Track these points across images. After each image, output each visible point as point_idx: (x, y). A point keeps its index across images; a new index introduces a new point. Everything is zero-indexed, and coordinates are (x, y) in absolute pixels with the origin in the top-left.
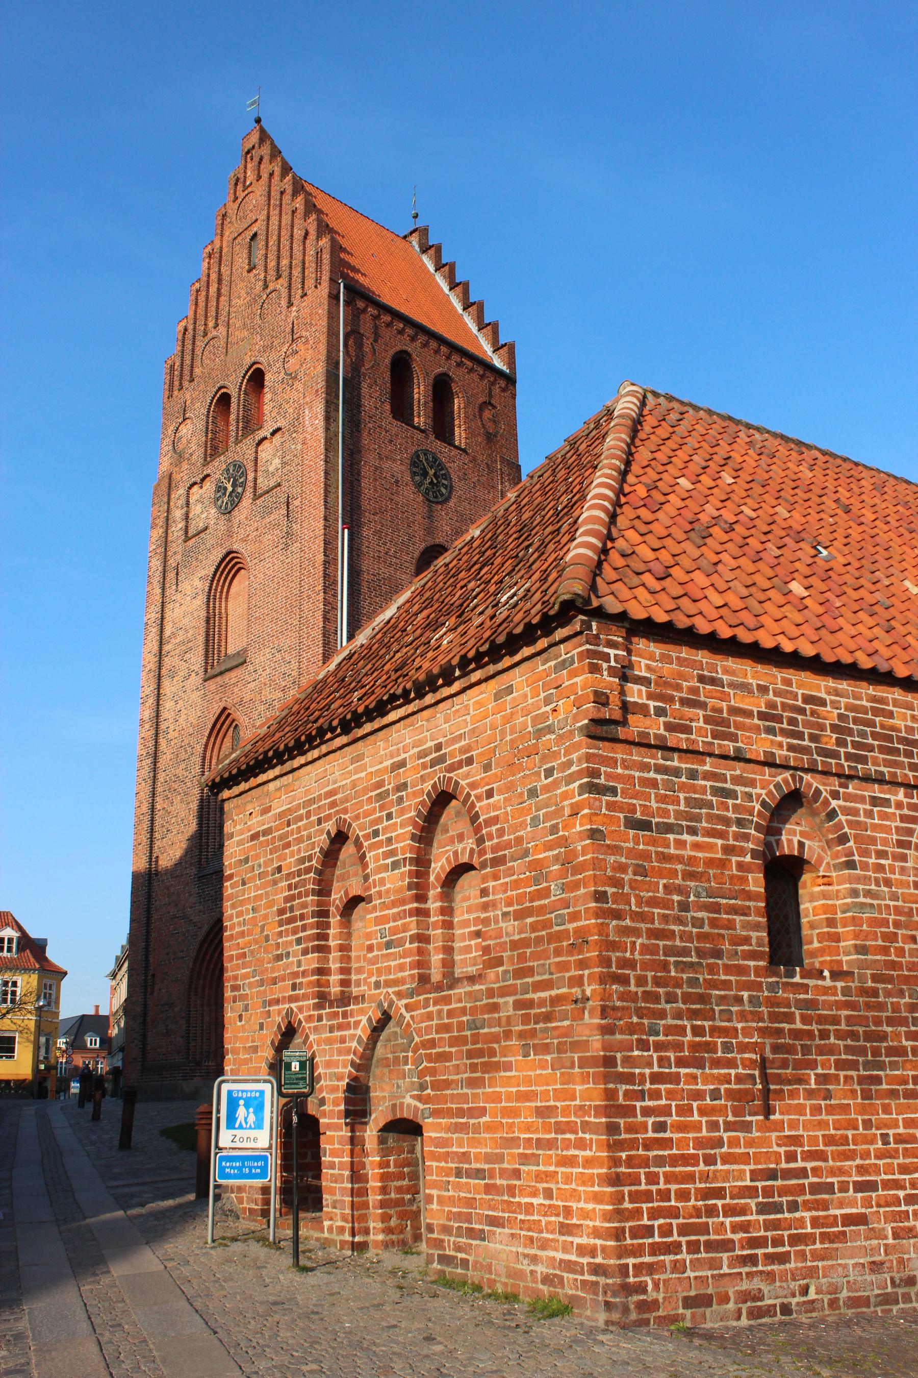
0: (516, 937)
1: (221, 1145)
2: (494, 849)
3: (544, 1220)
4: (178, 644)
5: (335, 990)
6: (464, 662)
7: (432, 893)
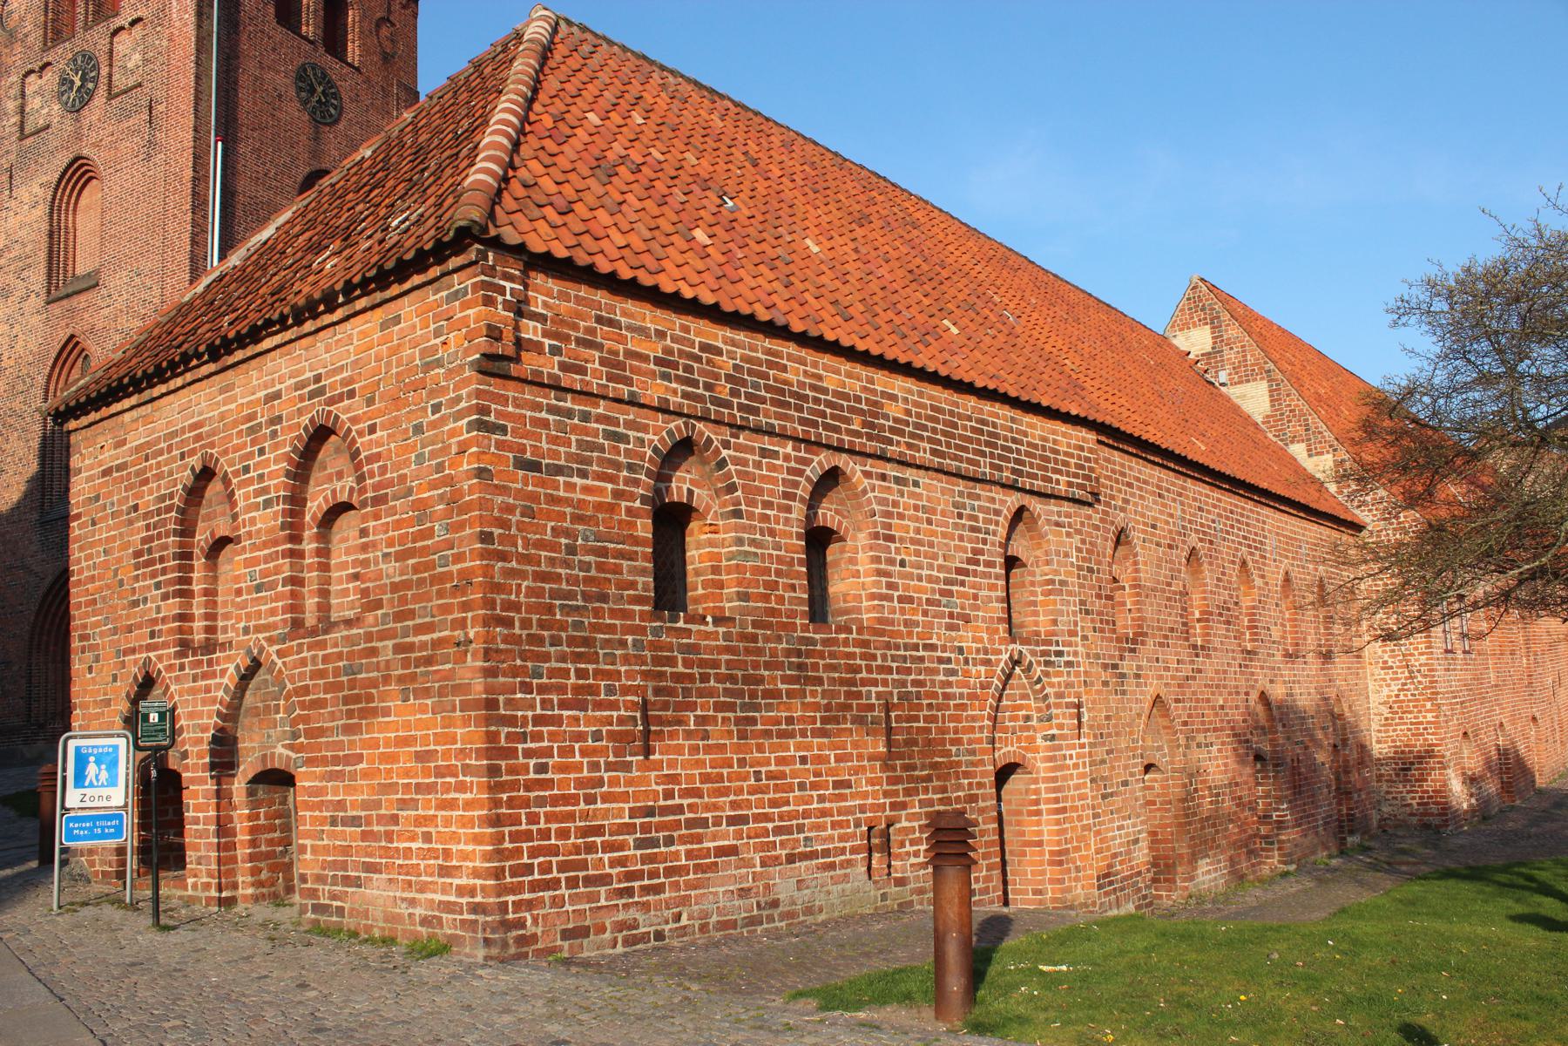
0: (397, 579)
1: (68, 805)
2: (376, 487)
3: (423, 864)
4: (14, 259)
5: (199, 637)
6: (349, 288)
7: (307, 534)
